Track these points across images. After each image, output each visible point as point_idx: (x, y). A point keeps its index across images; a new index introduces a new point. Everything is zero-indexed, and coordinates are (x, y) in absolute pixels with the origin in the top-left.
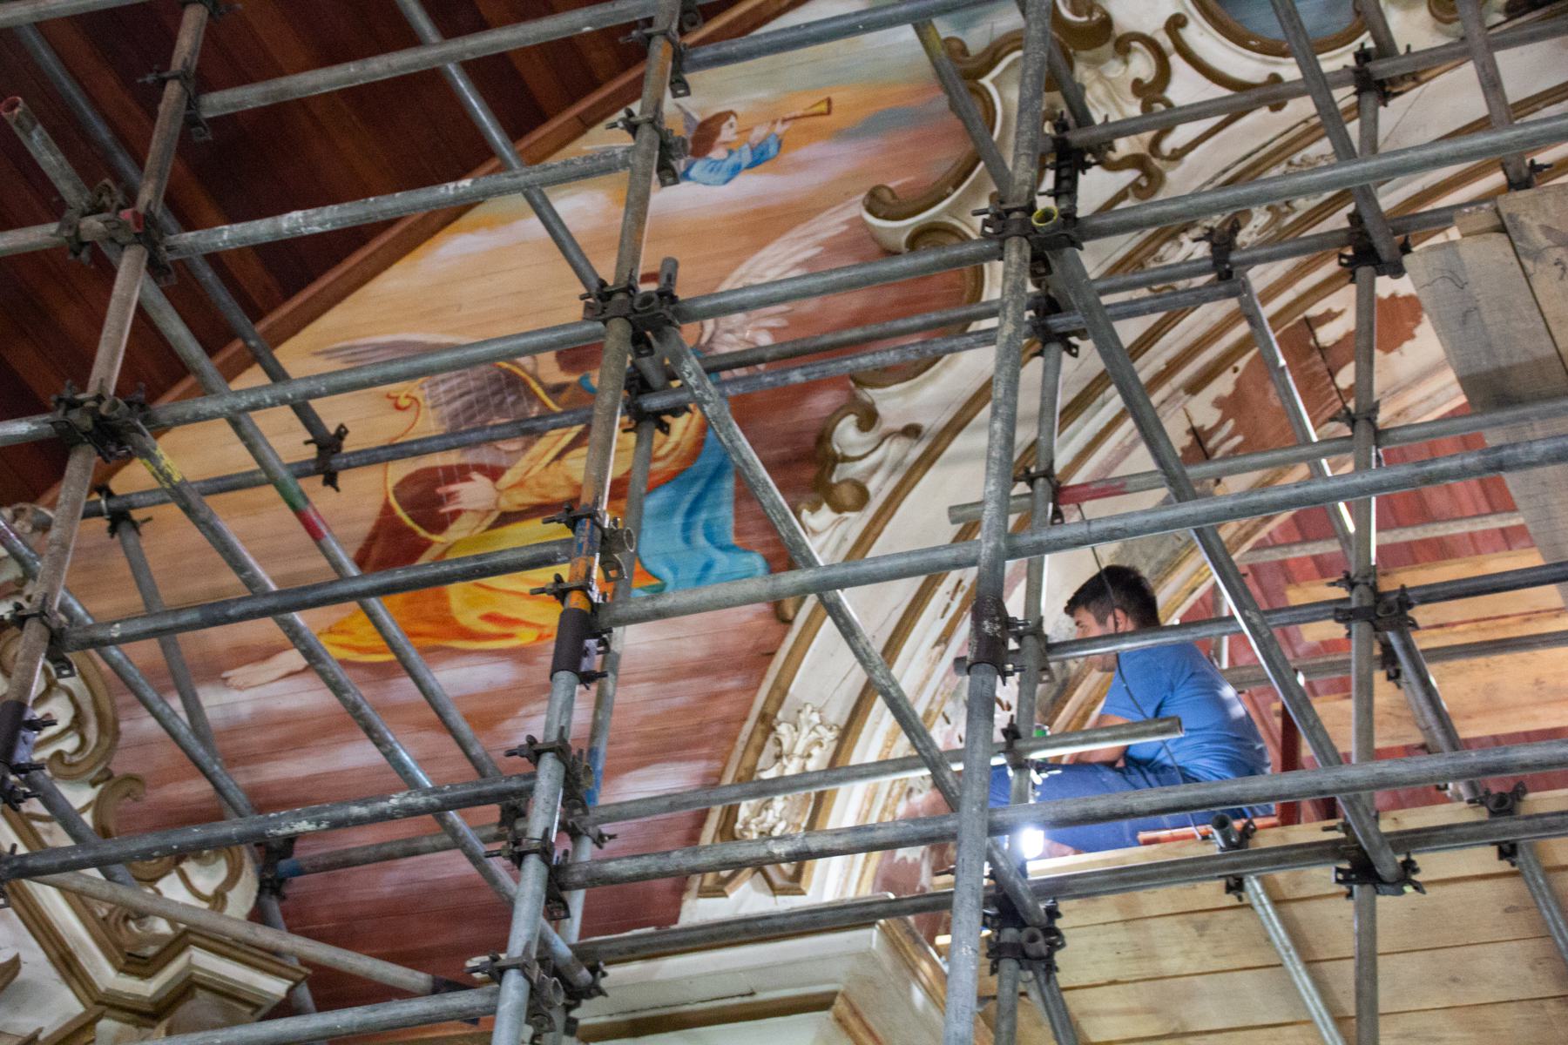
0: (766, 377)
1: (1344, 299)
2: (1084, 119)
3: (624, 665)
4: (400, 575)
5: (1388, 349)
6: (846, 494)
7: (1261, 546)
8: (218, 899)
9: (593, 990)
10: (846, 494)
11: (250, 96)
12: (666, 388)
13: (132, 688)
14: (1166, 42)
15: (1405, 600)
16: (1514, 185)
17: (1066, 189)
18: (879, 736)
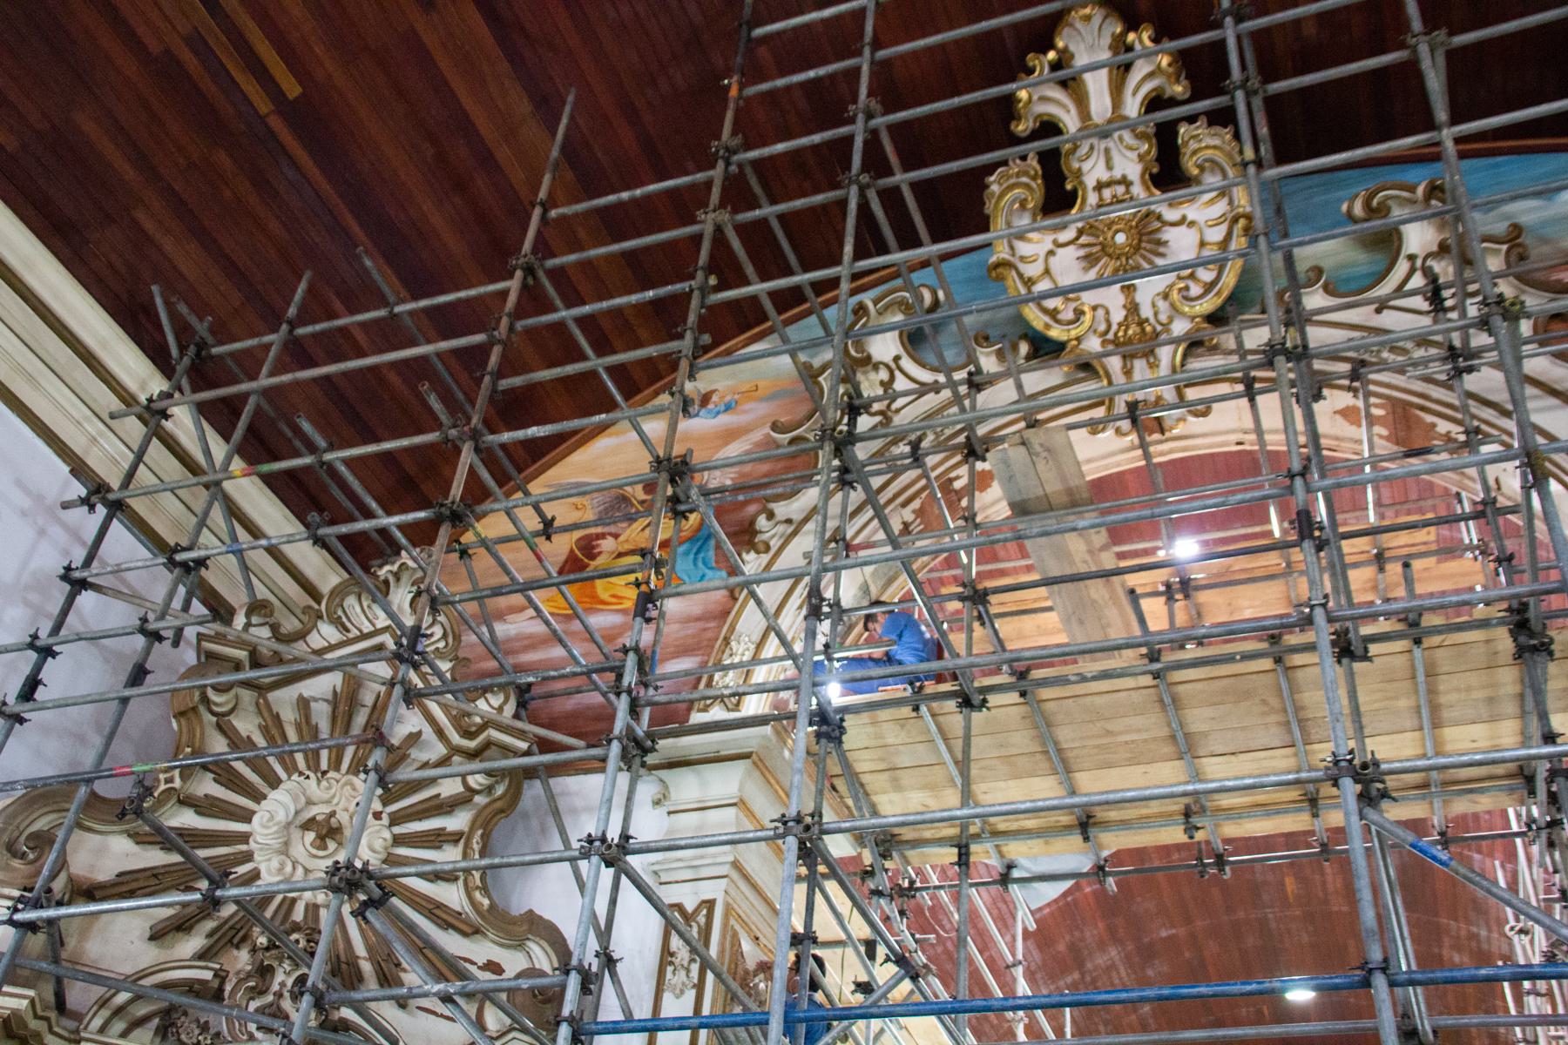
0: (729, 497)
1: (963, 471)
2: (860, 395)
3: (668, 616)
4: (578, 576)
5: (982, 491)
6: (761, 547)
7: (931, 571)
8: (500, 709)
9: (653, 750)
10: (761, 547)
11: (517, 381)
12: (687, 502)
13: (466, 622)
14: (893, 366)
15: (986, 593)
16: (1029, 426)
17: (852, 423)
18: (772, 647)
